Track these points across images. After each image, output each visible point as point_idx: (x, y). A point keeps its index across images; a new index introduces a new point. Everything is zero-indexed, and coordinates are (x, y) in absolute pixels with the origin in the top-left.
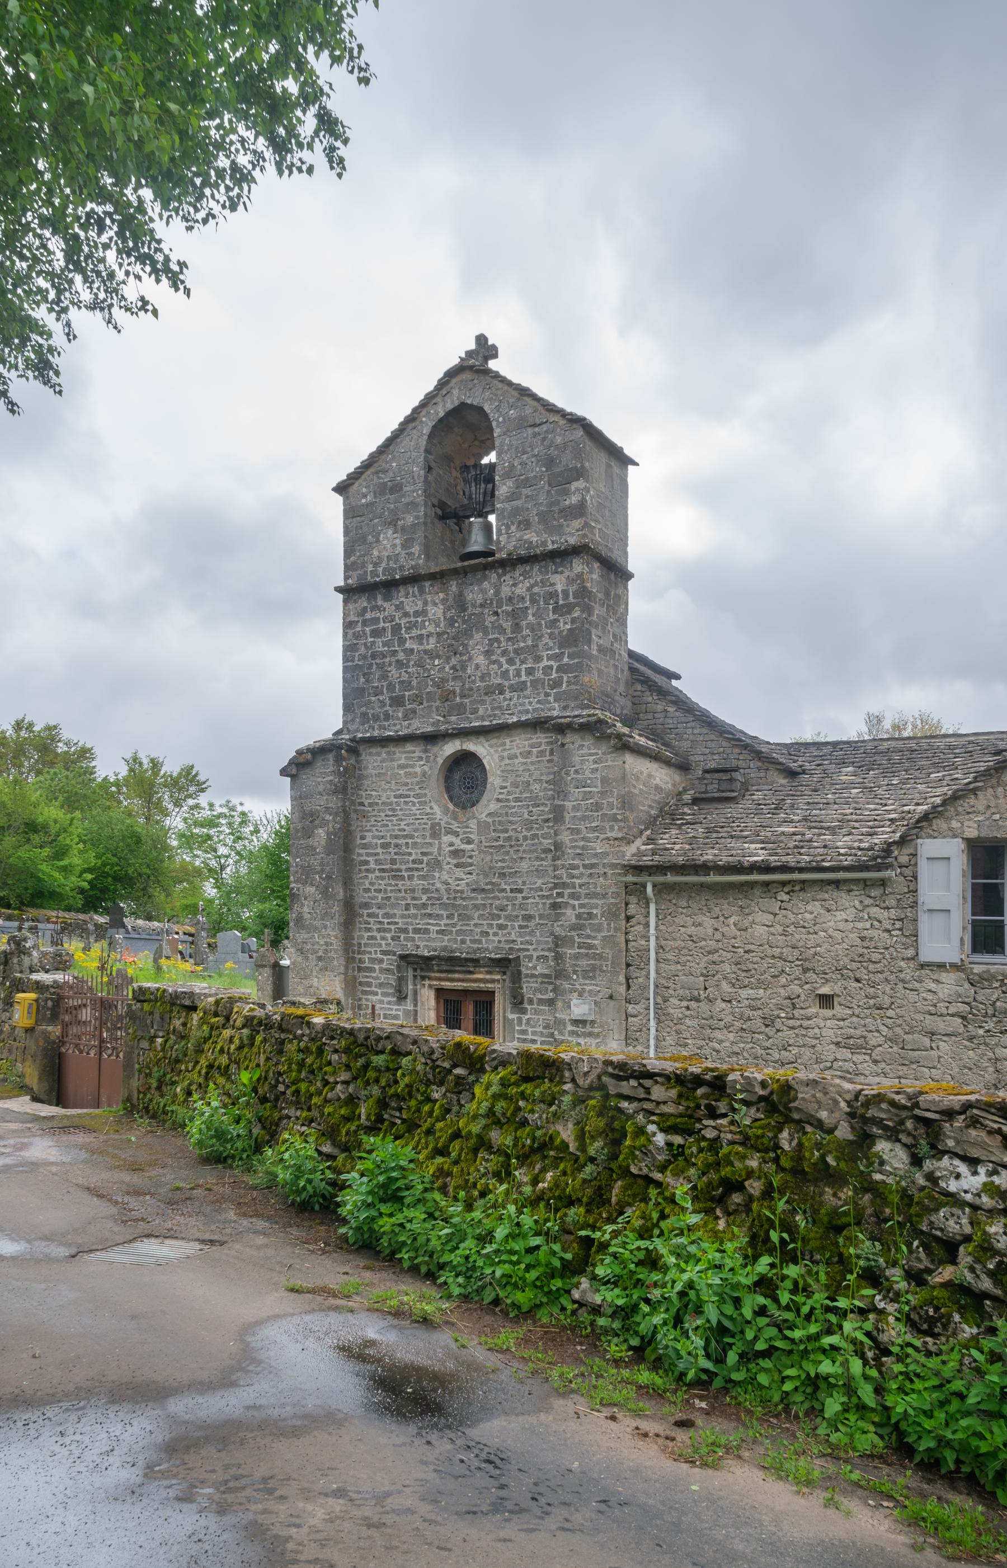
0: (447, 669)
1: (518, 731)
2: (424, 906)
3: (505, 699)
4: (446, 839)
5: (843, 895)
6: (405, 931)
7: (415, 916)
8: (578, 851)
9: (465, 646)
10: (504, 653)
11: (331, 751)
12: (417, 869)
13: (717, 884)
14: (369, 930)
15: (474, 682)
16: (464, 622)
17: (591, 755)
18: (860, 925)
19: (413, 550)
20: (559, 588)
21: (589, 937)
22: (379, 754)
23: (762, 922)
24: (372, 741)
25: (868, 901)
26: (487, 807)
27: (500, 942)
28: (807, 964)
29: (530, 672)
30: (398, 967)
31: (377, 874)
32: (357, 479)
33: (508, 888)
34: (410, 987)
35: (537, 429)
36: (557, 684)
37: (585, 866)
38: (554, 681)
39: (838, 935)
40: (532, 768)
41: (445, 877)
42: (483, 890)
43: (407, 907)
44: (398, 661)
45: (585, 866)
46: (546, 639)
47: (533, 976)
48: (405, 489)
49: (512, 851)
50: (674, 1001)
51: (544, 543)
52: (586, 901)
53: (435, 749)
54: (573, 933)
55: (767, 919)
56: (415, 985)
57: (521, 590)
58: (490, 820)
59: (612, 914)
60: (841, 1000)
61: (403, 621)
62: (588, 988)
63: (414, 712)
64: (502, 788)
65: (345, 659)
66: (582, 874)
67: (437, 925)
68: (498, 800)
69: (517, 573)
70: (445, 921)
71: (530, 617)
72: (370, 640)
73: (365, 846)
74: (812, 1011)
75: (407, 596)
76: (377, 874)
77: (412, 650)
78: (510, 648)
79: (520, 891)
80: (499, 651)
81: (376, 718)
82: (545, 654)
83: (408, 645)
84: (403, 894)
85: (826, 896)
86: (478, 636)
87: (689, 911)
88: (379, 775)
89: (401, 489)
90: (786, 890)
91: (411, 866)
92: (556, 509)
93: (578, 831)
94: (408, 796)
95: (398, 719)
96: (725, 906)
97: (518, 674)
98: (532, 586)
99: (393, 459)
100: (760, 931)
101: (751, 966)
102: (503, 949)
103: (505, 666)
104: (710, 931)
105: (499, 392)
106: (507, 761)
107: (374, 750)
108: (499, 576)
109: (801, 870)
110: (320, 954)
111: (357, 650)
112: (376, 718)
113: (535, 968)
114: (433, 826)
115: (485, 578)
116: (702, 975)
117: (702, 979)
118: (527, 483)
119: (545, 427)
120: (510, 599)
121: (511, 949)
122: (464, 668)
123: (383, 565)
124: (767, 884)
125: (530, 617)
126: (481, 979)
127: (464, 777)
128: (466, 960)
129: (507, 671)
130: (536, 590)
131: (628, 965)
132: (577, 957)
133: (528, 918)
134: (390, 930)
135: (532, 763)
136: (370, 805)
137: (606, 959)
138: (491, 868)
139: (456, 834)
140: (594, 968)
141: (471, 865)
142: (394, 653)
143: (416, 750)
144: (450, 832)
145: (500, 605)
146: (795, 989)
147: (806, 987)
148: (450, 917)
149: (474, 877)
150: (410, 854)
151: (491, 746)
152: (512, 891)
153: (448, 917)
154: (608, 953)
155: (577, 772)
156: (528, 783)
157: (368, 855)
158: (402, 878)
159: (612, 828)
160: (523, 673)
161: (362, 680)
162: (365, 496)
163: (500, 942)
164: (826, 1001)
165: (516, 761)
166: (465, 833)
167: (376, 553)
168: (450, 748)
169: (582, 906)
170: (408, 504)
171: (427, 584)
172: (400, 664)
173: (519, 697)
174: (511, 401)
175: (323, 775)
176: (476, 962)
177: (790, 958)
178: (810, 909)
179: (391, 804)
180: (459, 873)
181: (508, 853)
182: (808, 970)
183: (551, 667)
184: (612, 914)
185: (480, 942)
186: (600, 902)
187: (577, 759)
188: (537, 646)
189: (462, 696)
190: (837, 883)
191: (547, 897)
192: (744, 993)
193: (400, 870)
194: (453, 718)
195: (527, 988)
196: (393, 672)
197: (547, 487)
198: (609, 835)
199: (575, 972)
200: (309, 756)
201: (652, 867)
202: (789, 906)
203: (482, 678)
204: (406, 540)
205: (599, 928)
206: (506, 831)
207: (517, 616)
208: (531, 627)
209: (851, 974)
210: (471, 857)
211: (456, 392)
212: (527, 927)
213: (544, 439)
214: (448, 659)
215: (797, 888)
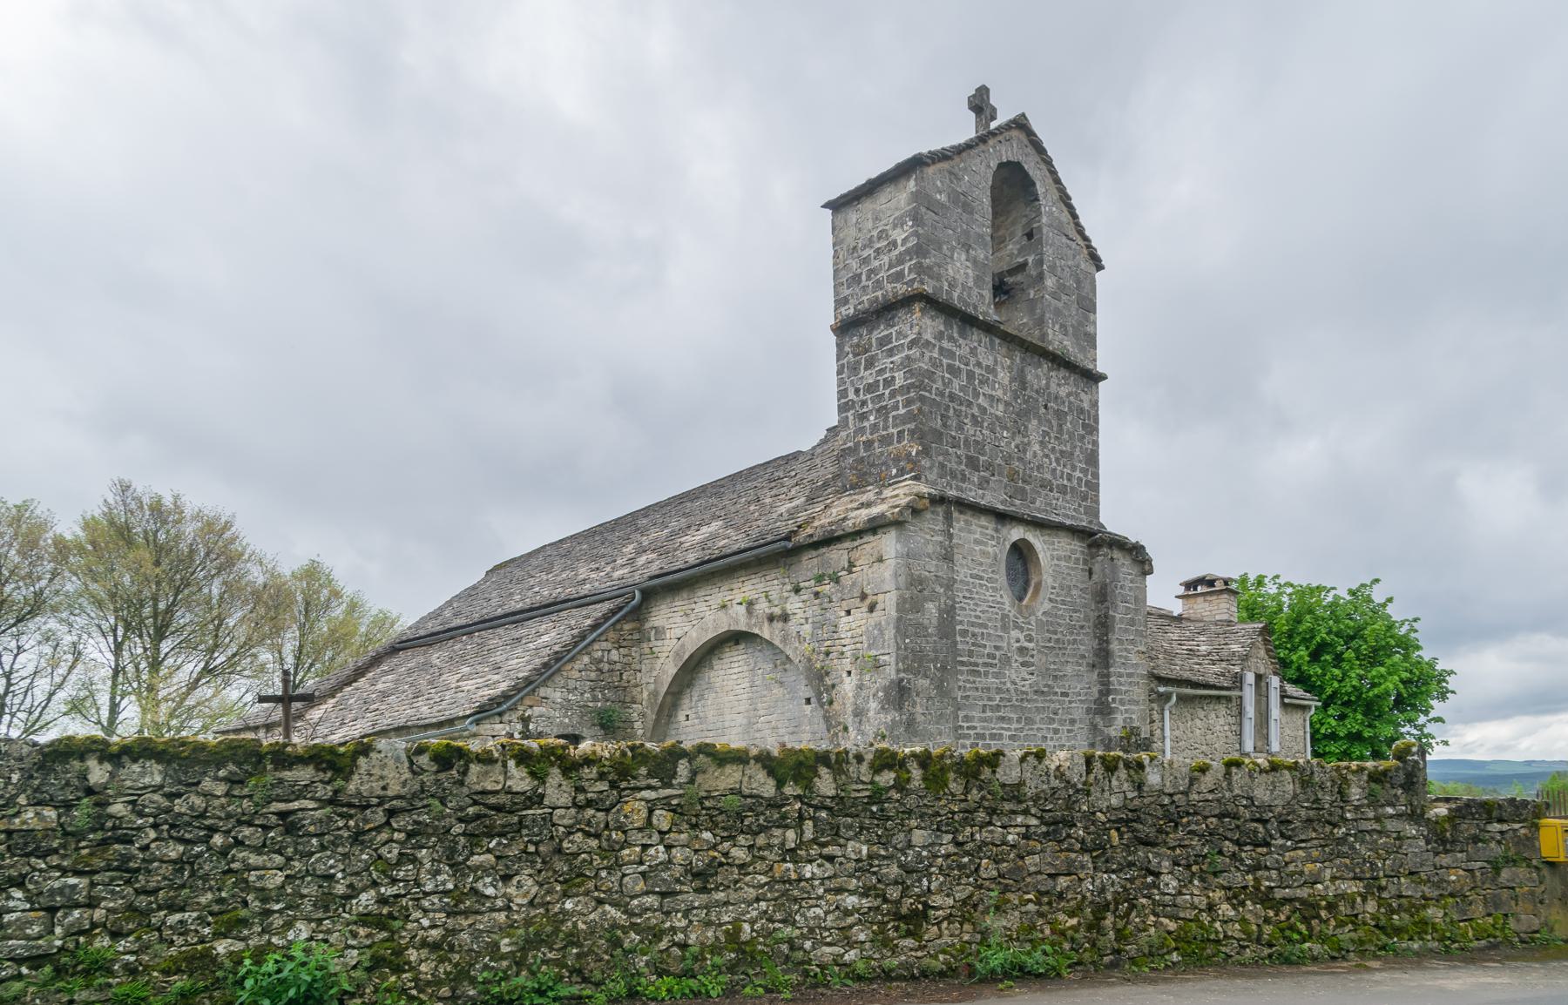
4: (1015, 633)
67: (1008, 729)
70: (1014, 726)
81: (953, 474)
115: (1040, 365)
133: (1073, 722)
139: (1022, 629)
144: (1017, 626)
148: (1019, 721)
180: (1024, 672)
193: (977, 665)
196: (969, 428)
208: (1069, 432)
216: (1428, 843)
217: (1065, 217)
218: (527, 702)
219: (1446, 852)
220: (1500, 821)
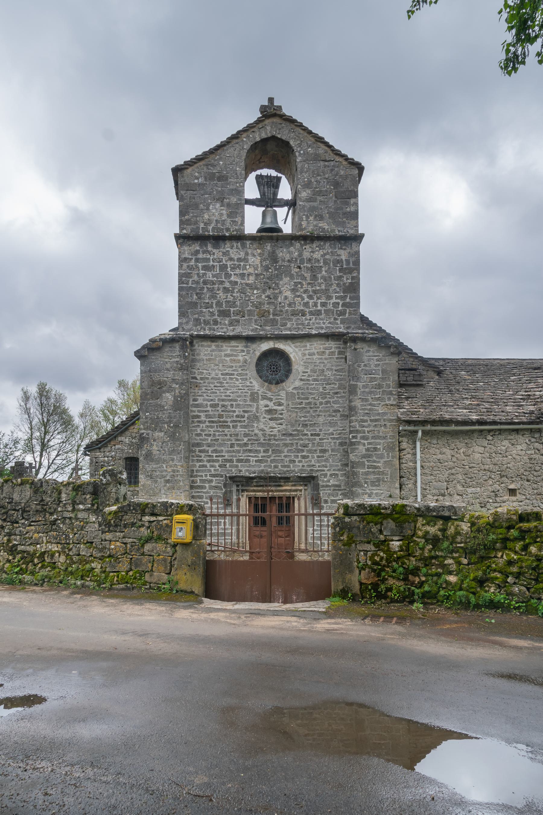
0: (263, 297)
1: (316, 339)
2: (246, 445)
3: (306, 319)
4: (262, 403)
5: (521, 437)
6: (231, 461)
7: (239, 451)
8: (366, 412)
9: (277, 284)
10: (306, 291)
11: (178, 341)
12: (240, 421)
13: (454, 431)
14: (200, 461)
15: (283, 307)
16: (276, 269)
17: (375, 356)
18: (529, 452)
19: (237, 219)
20: (344, 258)
21: (375, 462)
22: (210, 346)
23: (478, 451)
24: (205, 338)
25: (533, 440)
26: (292, 384)
27: (303, 466)
28: (503, 473)
29: (323, 305)
30: (225, 485)
31: (207, 424)
32: (191, 166)
33: (309, 433)
34: (235, 497)
35: (326, 163)
36: (342, 313)
37: (371, 421)
38: (340, 311)
39: (518, 457)
40: (326, 361)
41: (262, 426)
42: (291, 434)
43: (232, 445)
44: (225, 288)
45: (371, 421)
46: (334, 287)
47: (327, 486)
48: (230, 180)
49: (311, 411)
50: (430, 496)
51: (333, 231)
52: (373, 441)
53: (254, 346)
54: (364, 460)
55: (481, 449)
56: (238, 495)
57: (317, 255)
58: (294, 391)
59: (390, 448)
60: (520, 491)
61: (229, 263)
62: (375, 492)
63: (238, 321)
64: (304, 372)
65: (180, 282)
66: (369, 425)
68: (301, 380)
69: (314, 245)
70: (262, 454)
71: (324, 273)
72: (201, 272)
73: (197, 406)
74: (506, 498)
75: (232, 247)
76: (207, 424)
77: (236, 283)
78: (310, 289)
79: (318, 435)
80: (302, 290)
81: (206, 323)
82: (334, 295)
83: (232, 278)
84: (228, 437)
85: (512, 437)
86: (286, 279)
87: (438, 446)
88: (209, 360)
89: (227, 179)
90: (491, 434)
91: (235, 419)
92: (341, 212)
93: (367, 400)
94: (233, 375)
95: (226, 325)
96: (460, 443)
97: (315, 305)
98: (325, 254)
99: (220, 159)
100: (477, 456)
101: (473, 475)
102: (305, 470)
103: (306, 300)
104: (450, 457)
105: (301, 136)
106: (308, 357)
107: (205, 344)
108: (302, 245)
109: (501, 423)
110: (168, 478)
111: (191, 277)
112: (206, 323)
113: (329, 481)
114: (252, 394)
115: (292, 245)
116: (446, 481)
117: (446, 483)
118: (320, 193)
119: (332, 163)
120: (310, 260)
121: (311, 470)
122: (276, 298)
123: (213, 225)
124: (481, 431)
125: (324, 273)
126: (287, 490)
127: (274, 366)
128: (281, 478)
129: (308, 303)
130: (327, 257)
131: (401, 477)
132: (367, 473)
133: (324, 451)
134: (218, 461)
135: (326, 359)
136: (202, 379)
137: (387, 474)
138: (296, 421)
139: (271, 400)
140: (378, 480)
141: (282, 419)
142: (222, 282)
143: (240, 345)
144: (264, 398)
145: (302, 261)
146: (496, 486)
147: (503, 485)
149: (284, 426)
150: (234, 411)
151: (296, 347)
152: (312, 435)
153: (264, 452)
154: (388, 470)
155: (365, 365)
156: (323, 371)
157: (199, 411)
158: (228, 427)
159: (389, 399)
160: (319, 305)
161: (195, 297)
162: (197, 178)
163: (303, 466)
164: (512, 492)
165: (315, 357)
166: (277, 399)
167: (206, 216)
168: (265, 346)
169: (369, 444)
170: (233, 190)
171: (248, 242)
172: (226, 290)
173: (316, 319)
174: (309, 143)
175: (172, 357)
176: (287, 479)
177: (494, 470)
178: (504, 444)
179: (219, 379)
180: (273, 424)
181: (309, 412)
182: (504, 476)
183: (338, 304)
184: (390, 448)
185: (289, 466)
186: (382, 441)
187: (365, 358)
188: (329, 290)
189: (274, 315)
190: (517, 431)
191: (337, 439)
192: (470, 490)
193: (227, 422)
194: (268, 328)
195: (323, 494)
196: (221, 295)
197: (334, 198)
198: (387, 402)
199: (366, 483)
200: (161, 344)
201: (417, 421)
202: (492, 443)
203: (290, 305)
204: (231, 213)
205: (381, 456)
206: (308, 399)
207: (314, 271)
209: (525, 478)
210: (281, 414)
211: (269, 128)
212: (323, 456)
213: (332, 170)
214: (264, 291)
215: (497, 433)
216: (100, 525)
217: (322, 149)
218: (112, 443)
219: (109, 531)
220: (153, 514)
